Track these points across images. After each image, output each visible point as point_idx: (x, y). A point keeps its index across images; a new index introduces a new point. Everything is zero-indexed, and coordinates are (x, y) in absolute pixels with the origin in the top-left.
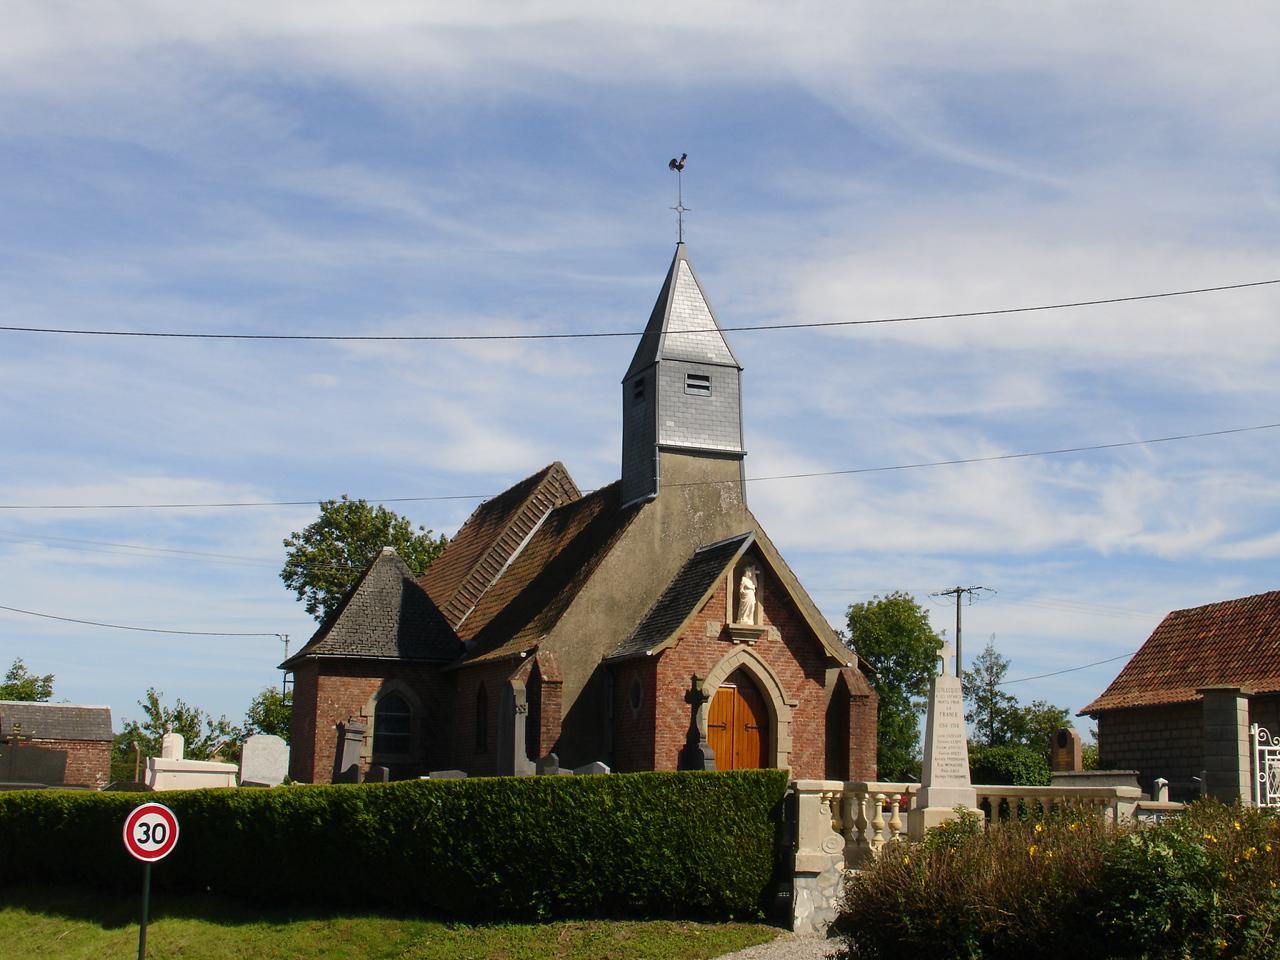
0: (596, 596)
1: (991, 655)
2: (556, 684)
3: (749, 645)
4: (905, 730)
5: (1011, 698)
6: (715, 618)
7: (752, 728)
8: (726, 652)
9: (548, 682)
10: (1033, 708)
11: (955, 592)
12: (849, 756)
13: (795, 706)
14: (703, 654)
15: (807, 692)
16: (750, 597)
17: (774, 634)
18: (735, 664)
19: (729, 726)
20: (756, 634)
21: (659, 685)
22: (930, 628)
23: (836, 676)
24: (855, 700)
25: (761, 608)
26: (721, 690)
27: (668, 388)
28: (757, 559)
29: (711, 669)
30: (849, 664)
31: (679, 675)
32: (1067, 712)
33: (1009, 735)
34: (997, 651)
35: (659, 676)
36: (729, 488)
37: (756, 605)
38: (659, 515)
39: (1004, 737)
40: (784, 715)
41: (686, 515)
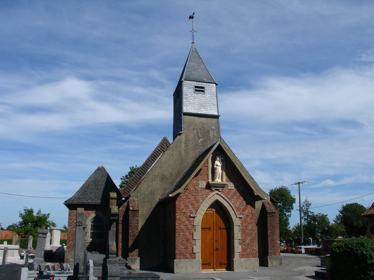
0: (156, 174)
1: (306, 201)
2: (136, 211)
3: (219, 191)
4: (285, 222)
5: (312, 212)
6: (203, 179)
7: (223, 228)
8: (209, 194)
9: (132, 210)
10: (318, 215)
11: (298, 183)
12: (268, 238)
13: (242, 218)
14: (197, 196)
15: (247, 211)
16: (219, 170)
17: (231, 186)
18: (213, 200)
19: (212, 228)
20: (223, 186)
21: (177, 210)
22: (291, 195)
23: (261, 205)
24: (269, 214)
25: (224, 174)
26: (207, 212)
27: (187, 91)
28: (221, 152)
29: (202, 203)
30: (265, 198)
31: (187, 205)
32: (327, 215)
33: (312, 222)
34: (308, 200)
35: (177, 206)
36: (213, 129)
37: (222, 173)
38: (183, 140)
39: (311, 222)
40: (237, 222)
41: (195, 140)
